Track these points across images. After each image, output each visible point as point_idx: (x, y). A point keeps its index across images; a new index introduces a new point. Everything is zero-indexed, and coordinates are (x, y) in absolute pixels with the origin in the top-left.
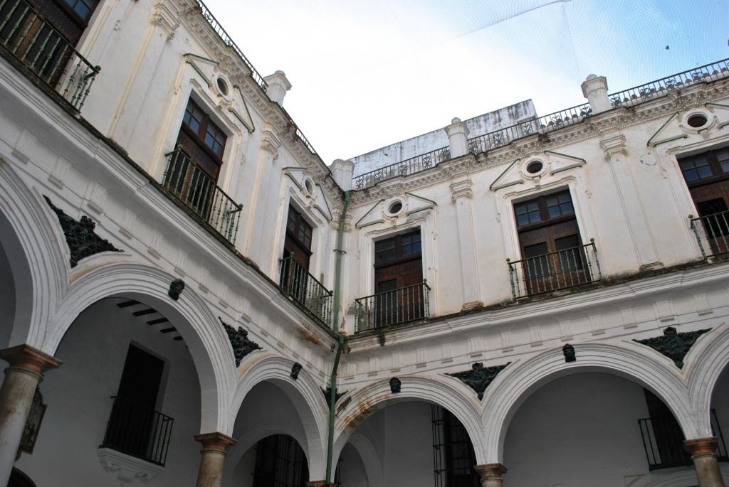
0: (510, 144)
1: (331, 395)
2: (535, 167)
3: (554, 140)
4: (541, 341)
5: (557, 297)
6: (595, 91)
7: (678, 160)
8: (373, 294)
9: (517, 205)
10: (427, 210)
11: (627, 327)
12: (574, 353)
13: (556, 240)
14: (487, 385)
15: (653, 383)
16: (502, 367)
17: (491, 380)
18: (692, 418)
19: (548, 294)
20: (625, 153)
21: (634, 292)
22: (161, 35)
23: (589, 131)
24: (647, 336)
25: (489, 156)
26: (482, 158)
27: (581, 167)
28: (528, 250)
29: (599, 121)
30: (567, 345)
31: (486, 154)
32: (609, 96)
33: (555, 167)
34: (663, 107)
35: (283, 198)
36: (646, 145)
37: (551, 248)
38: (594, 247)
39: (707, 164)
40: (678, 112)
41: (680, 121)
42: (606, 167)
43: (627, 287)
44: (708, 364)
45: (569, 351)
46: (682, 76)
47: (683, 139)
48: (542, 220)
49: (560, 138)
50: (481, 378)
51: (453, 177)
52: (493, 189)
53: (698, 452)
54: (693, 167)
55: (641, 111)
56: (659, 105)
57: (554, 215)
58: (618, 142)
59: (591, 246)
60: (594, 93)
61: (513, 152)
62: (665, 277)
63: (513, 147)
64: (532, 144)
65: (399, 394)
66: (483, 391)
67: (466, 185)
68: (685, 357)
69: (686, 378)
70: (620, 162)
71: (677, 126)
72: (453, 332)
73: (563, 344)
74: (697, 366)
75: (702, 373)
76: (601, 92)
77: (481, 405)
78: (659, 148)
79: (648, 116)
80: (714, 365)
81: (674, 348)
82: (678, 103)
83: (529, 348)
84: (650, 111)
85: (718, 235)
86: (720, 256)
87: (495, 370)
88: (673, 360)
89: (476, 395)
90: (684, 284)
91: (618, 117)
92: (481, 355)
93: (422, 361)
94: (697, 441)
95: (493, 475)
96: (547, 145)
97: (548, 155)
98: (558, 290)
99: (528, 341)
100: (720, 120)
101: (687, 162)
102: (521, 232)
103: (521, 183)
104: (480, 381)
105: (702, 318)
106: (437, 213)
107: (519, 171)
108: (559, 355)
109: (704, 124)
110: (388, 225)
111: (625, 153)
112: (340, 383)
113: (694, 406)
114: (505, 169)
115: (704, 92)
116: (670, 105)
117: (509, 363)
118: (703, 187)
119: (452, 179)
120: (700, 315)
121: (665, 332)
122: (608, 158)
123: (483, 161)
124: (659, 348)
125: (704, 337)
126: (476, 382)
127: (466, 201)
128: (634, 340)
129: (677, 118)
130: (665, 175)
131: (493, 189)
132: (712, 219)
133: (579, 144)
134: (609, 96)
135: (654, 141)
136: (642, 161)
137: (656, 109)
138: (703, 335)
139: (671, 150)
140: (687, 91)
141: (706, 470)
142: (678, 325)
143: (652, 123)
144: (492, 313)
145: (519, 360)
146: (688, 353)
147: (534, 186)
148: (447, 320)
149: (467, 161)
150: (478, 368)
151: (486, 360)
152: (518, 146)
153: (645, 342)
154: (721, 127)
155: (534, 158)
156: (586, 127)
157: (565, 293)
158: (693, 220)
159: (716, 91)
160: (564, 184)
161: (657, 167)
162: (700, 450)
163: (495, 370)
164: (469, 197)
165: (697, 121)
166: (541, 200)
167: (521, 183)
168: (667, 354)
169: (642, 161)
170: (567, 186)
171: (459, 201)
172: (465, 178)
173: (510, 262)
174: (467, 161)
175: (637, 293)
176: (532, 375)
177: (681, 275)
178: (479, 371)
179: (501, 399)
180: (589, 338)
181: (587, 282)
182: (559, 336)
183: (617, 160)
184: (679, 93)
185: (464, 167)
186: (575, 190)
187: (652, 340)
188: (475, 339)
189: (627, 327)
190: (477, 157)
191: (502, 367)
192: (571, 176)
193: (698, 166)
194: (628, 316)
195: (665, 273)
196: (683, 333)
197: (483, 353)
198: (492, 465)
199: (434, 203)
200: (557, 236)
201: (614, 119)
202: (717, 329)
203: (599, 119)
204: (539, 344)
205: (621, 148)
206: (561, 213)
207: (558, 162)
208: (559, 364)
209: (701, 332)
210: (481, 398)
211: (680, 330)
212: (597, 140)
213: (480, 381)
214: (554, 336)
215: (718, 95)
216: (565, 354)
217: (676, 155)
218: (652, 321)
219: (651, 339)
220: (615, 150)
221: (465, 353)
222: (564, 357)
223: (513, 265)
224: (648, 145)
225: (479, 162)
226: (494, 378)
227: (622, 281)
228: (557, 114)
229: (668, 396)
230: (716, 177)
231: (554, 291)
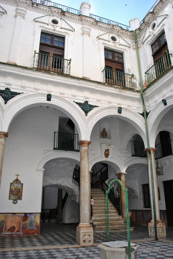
0: (49, 6)
1: (145, 115)
3: (66, 16)
4: (39, 89)
5: (52, 74)
6: (86, 8)
7: (41, 32)
9: (43, 33)
10: (1, 13)
11: (72, 96)
12: (51, 98)
13: (53, 54)
14: (10, 99)
15: (76, 118)
16: (19, 94)
17: (13, 97)
18: (85, 133)
19: (49, 72)
20: (89, 35)
21: (80, 84)
23: (80, 21)
24: (79, 101)
25: (38, 7)
26: (35, 5)
27: (72, 32)
28: (42, 52)
29: (85, 19)
30: (50, 94)
31: (37, 4)
33: (63, 26)
34: (106, 28)
36: (96, 37)
38: (70, 62)
39: (111, 54)
40: (50, 15)
41: (109, 36)
42: (81, 36)
43: (79, 82)
44: (95, 117)
45: (49, 96)
46: (61, 6)
47: (108, 42)
48: (51, 43)
49: (69, 17)
50: (8, 95)
51: (18, 6)
52: (35, 20)
53: (84, 145)
55: (100, 24)
56: (105, 26)
58: (88, 30)
59: (69, 61)
60: (85, 8)
61: (49, 11)
62: (92, 83)
63: (50, 9)
64: (58, 12)
65: (121, 114)
66: (8, 101)
67: (24, 12)
68: (89, 113)
69: (6, 108)
70: (86, 37)
71: (108, 37)
72: (80, 86)
73: (48, 93)
74: (91, 117)
75: (92, 120)
76: (87, 10)
77: (5, 106)
78: (100, 40)
79: (100, 28)
80: (96, 118)
81: (86, 109)
82: (111, 29)
83: (33, 90)
84: (102, 26)
85: (109, 78)
87: (15, 94)
88: (85, 112)
89: (4, 101)
90: (96, 88)
91: (92, 22)
92: (11, 85)
93: (50, 90)
94: (85, 141)
95: (3, 137)
96: (63, 16)
97: (62, 20)
98: (53, 72)
99: (33, 87)
100: (18, 17)
101: (44, 34)
102: (41, 44)
103: (48, 25)
104: (8, 96)
106: (5, 17)
107: (48, 20)
108: (45, 97)
111: (89, 35)
112: (148, 109)
113: (87, 130)
114: (43, 16)
116: (108, 28)
117: (22, 93)
118: (108, 61)
119: (18, 6)
120: (97, 101)
121: (6, 89)
122: (83, 34)
123: (35, 7)
124: (81, 107)
125: (96, 108)
126: (6, 96)
127: (22, 19)
128: (74, 101)
129: (109, 34)
130: (34, 34)
131: (35, 20)
133: (74, 23)
136: (93, 42)
137: (104, 27)
138: (96, 107)
139: (104, 43)
140: (116, 27)
141: (85, 151)
142: (89, 101)
143: (101, 31)
144: (22, 69)
145: (27, 93)
146: (90, 112)
147: (53, 29)
148: (79, 80)
149: (28, 2)
150: (8, 90)
151: (12, 88)
152: (52, 9)
153: (77, 103)
154: (120, 45)
155: (55, 18)
156: (79, 18)
157: (56, 74)
158: (36, 53)
159: (123, 33)
160: (123, 51)
161: (97, 46)
162: (85, 144)
163: (15, 94)
164: (23, 18)
165: (113, 39)
166: (53, 36)
168: (83, 110)
169: (93, 42)
171: (18, 17)
173: (36, 52)
174: (28, 2)
175: (81, 85)
176: (31, 101)
177: (97, 85)
178: (8, 91)
179: (15, 106)
180: (58, 94)
181: (62, 73)
182: (47, 89)
183: (86, 37)
184: (113, 26)
185: (25, 4)
186: (68, 39)
187: (146, 116)
189: (72, 96)
190: (33, 4)
191: (19, 94)
192: (68, 33)
194: (74, 92)
195: (92, 82)
196: (91, 105)
197: (12, 85)
198: (4, 132)
199: (6, 12)
200: (55, 53)
201: (90, 21)
202: (100, 107)
203: (85, 18)
204: (38, 90)
205: (89, 33)
206: (46, 42)
207: (65, 25)
208: (44, 100)
209: (96, 106)
210: (6, 103)
211: (89, 103)
212: (81, 26)
213: (8, 96)
214: (46, 89)
215: (122, 34)
216: (47, 97)
217: (42, 30)
218: (81, 97)
219: (80, 103)
220: (87, 33)
221: (3, 82)
222: (46, 98)
224: (97, 38)
225: (33, 6)
226: (14, 97)
227: (77, 78)
229: (80, 124)
230: (113, 60)
231: (51, 71)
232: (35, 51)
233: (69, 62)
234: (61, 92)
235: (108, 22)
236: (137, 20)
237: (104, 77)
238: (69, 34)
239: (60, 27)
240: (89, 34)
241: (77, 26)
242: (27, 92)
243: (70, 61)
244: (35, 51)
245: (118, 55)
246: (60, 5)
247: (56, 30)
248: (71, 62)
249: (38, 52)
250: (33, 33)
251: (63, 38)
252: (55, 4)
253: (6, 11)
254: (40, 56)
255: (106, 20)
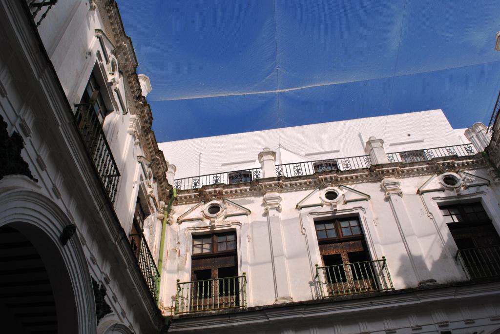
2: (331, 195)
8: (190, 281)
22: (86, 4)
32: (175, 180)
35: (136, 182)
37: (215, 273)
38: (384, 263)
54: (324, 229)
57: (222, 248)
67: (277, 200)
72: (421, 303)
86: (475, 281)
99: (409, 326)
105: (467, 326)
109: (335, 198)
110: (207, 222)
115: (338, 177)
132: (357, 266)
134: (175, 180)
135: (300, 205)
139: (311, 213)
147: (456, 194)
155: (330, 188)
158: (318, 268)
160: (355, 211)
166: (335, 220)
167: (321, 205)
170: (236, 228)
172: (277, 194)
173: (318, 267)
186: (365, 218)
188: (338, 327)
192: (239, 222)
193: (327, 228)
223: (181, 286)
228: (179, 181)
232: (317, 265)
233: (382, 263)
234: (413, 325)
235: (465, 148)
236: (480, 127)
237: (463, 268)
238: (241, 224)
239: (342, 202)
240: (279, 208)
241: (372, 188)
242: (482, 330)
243: (384, 260)
244: (317, 265)
245: (449, 212)
246: (355, 157)
247: (338, 209)
248: (386, 261)
249: (320, 263)
250: (302, 232)
251: (356, 217)
252: (295, 165)
253: (249, 209)
254: (197, 286)
255: (444, 149)
